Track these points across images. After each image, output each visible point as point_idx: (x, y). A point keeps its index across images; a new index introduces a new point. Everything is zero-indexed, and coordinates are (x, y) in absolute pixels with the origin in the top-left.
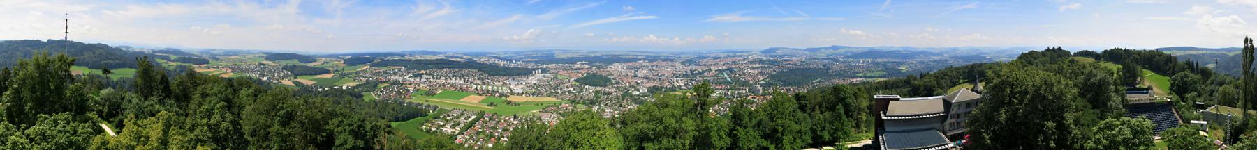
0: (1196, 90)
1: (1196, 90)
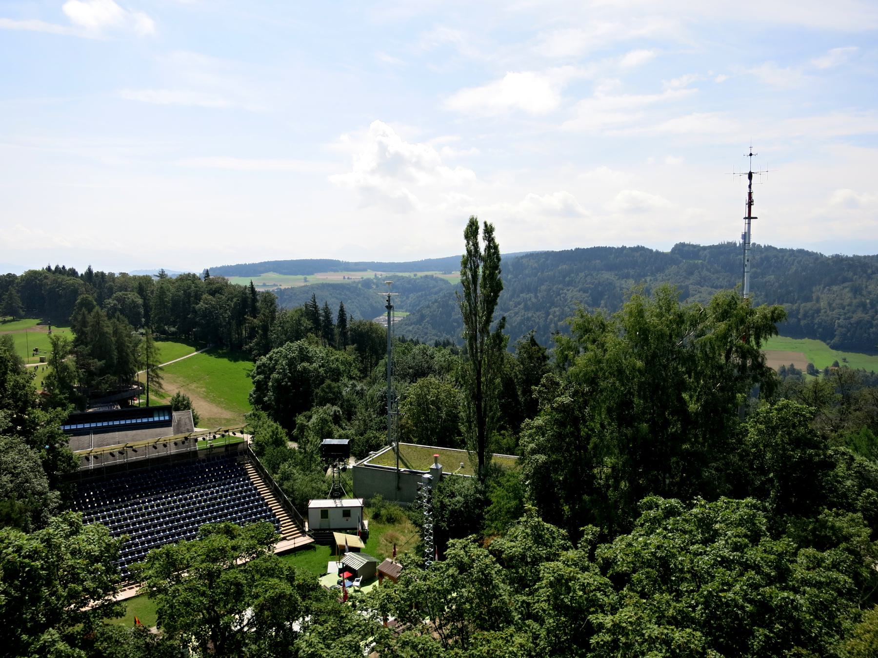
0: (335, 398)
1: (335, 398)
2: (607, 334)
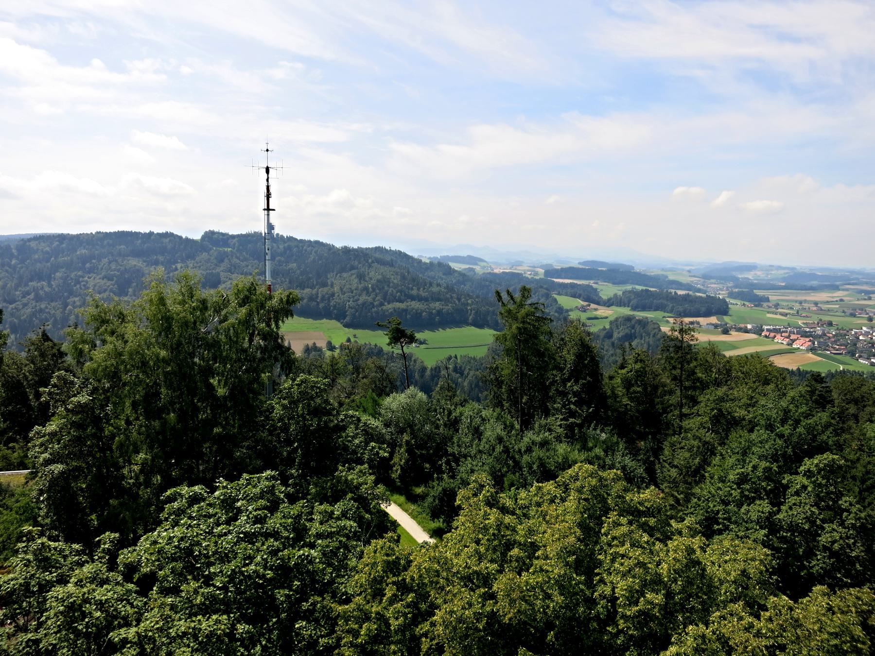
2: (126, 325)
